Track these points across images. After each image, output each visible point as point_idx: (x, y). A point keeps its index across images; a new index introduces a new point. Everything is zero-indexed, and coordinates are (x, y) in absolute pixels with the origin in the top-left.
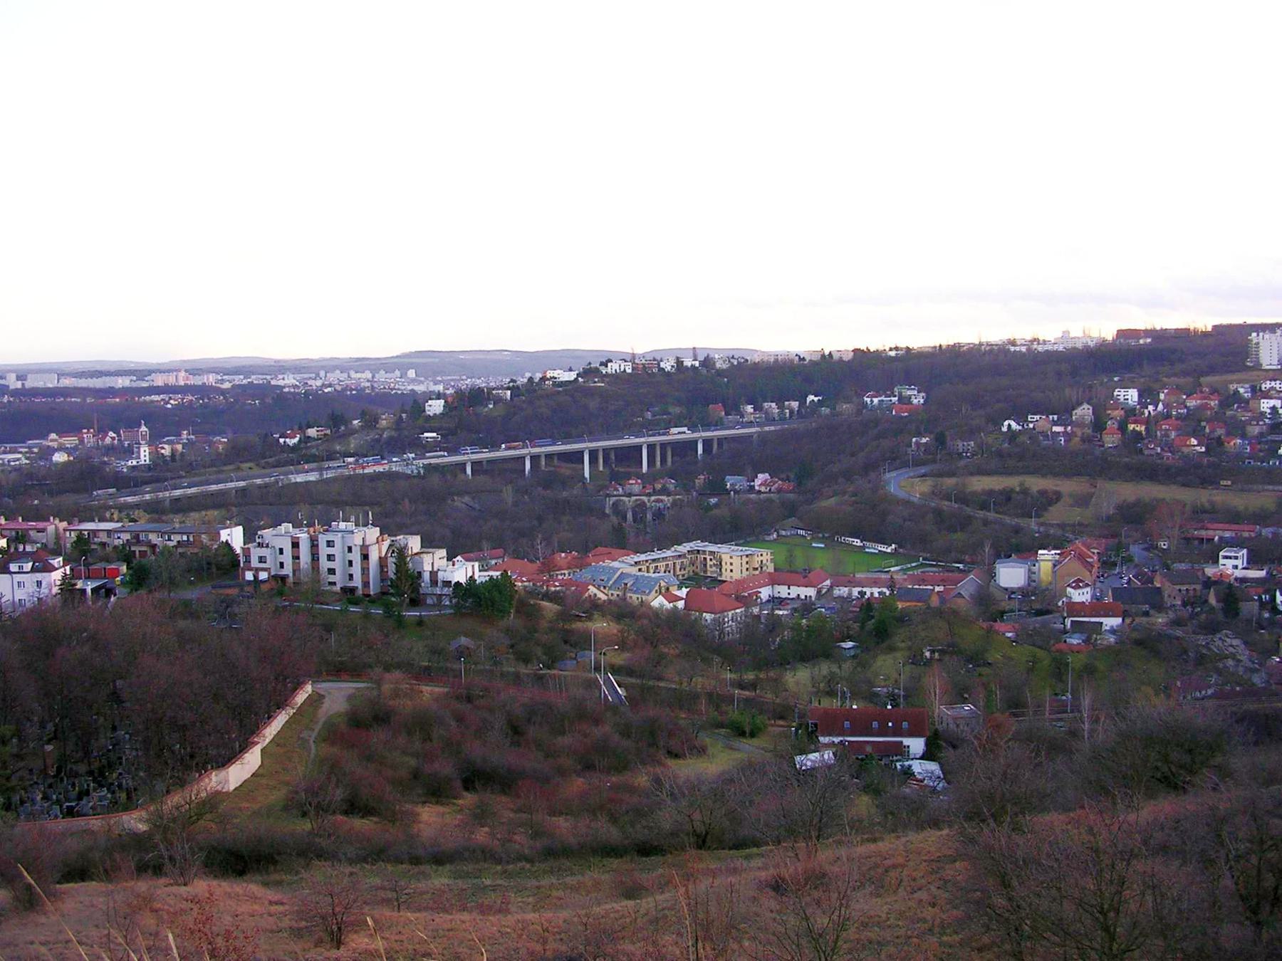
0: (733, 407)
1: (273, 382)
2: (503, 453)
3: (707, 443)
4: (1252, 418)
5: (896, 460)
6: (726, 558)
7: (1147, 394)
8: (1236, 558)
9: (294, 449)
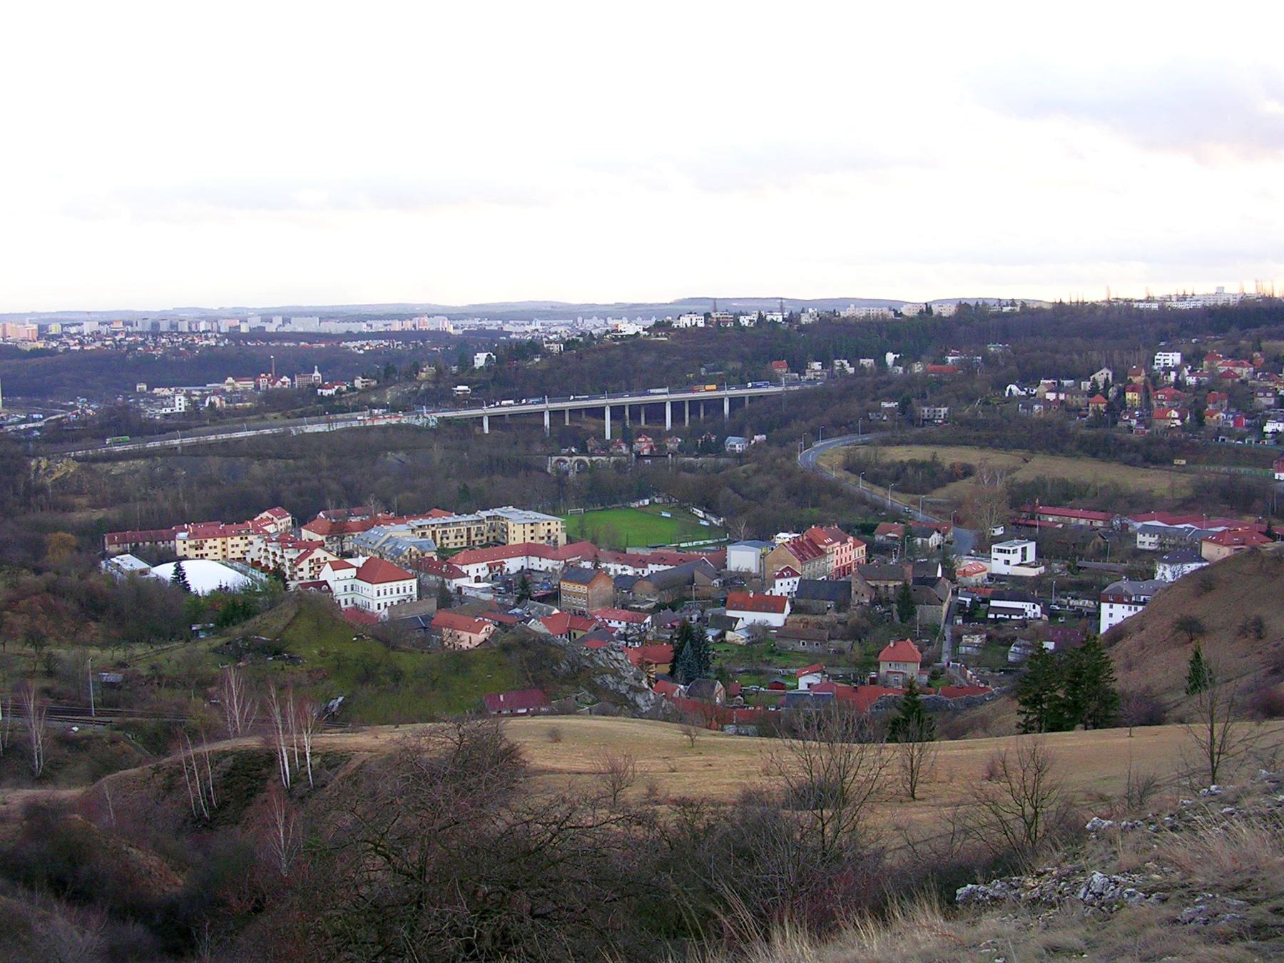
3: (736, 402)
9: (330, 397)
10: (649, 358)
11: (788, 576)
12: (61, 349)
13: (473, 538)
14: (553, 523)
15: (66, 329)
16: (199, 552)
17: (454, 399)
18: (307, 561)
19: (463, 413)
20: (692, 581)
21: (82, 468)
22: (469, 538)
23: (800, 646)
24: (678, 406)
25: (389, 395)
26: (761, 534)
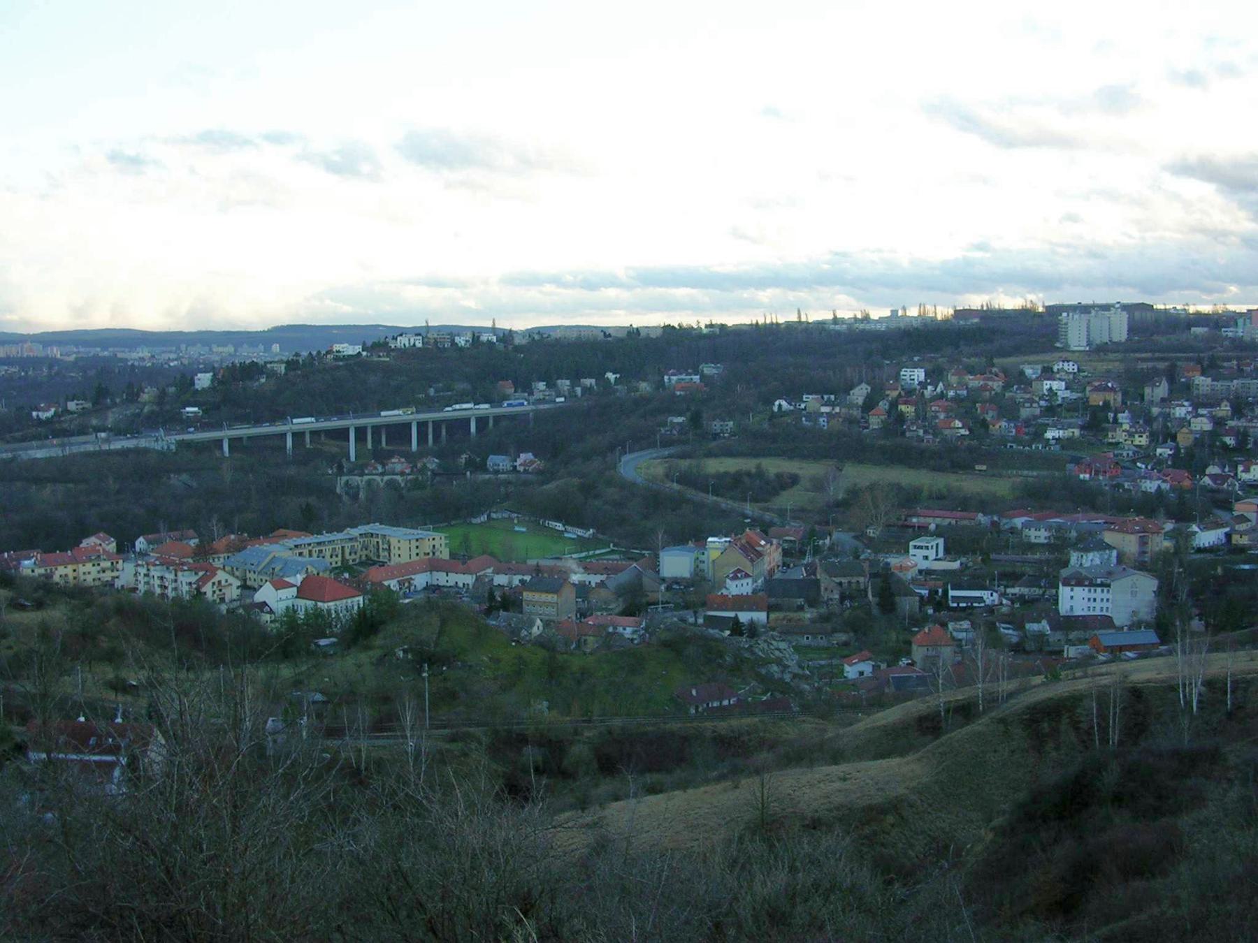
0: (525, 386)
1: (119, 355)
2: (266, 429)
4: (1028, 400)
5: (642, 440)
6: (394, 541)
7: (935, 375)
8: (927, 548)
9: (49, 421)
10: (373, 379)
14: (437, 538)
24: (361, 432)
25: (111, 418)
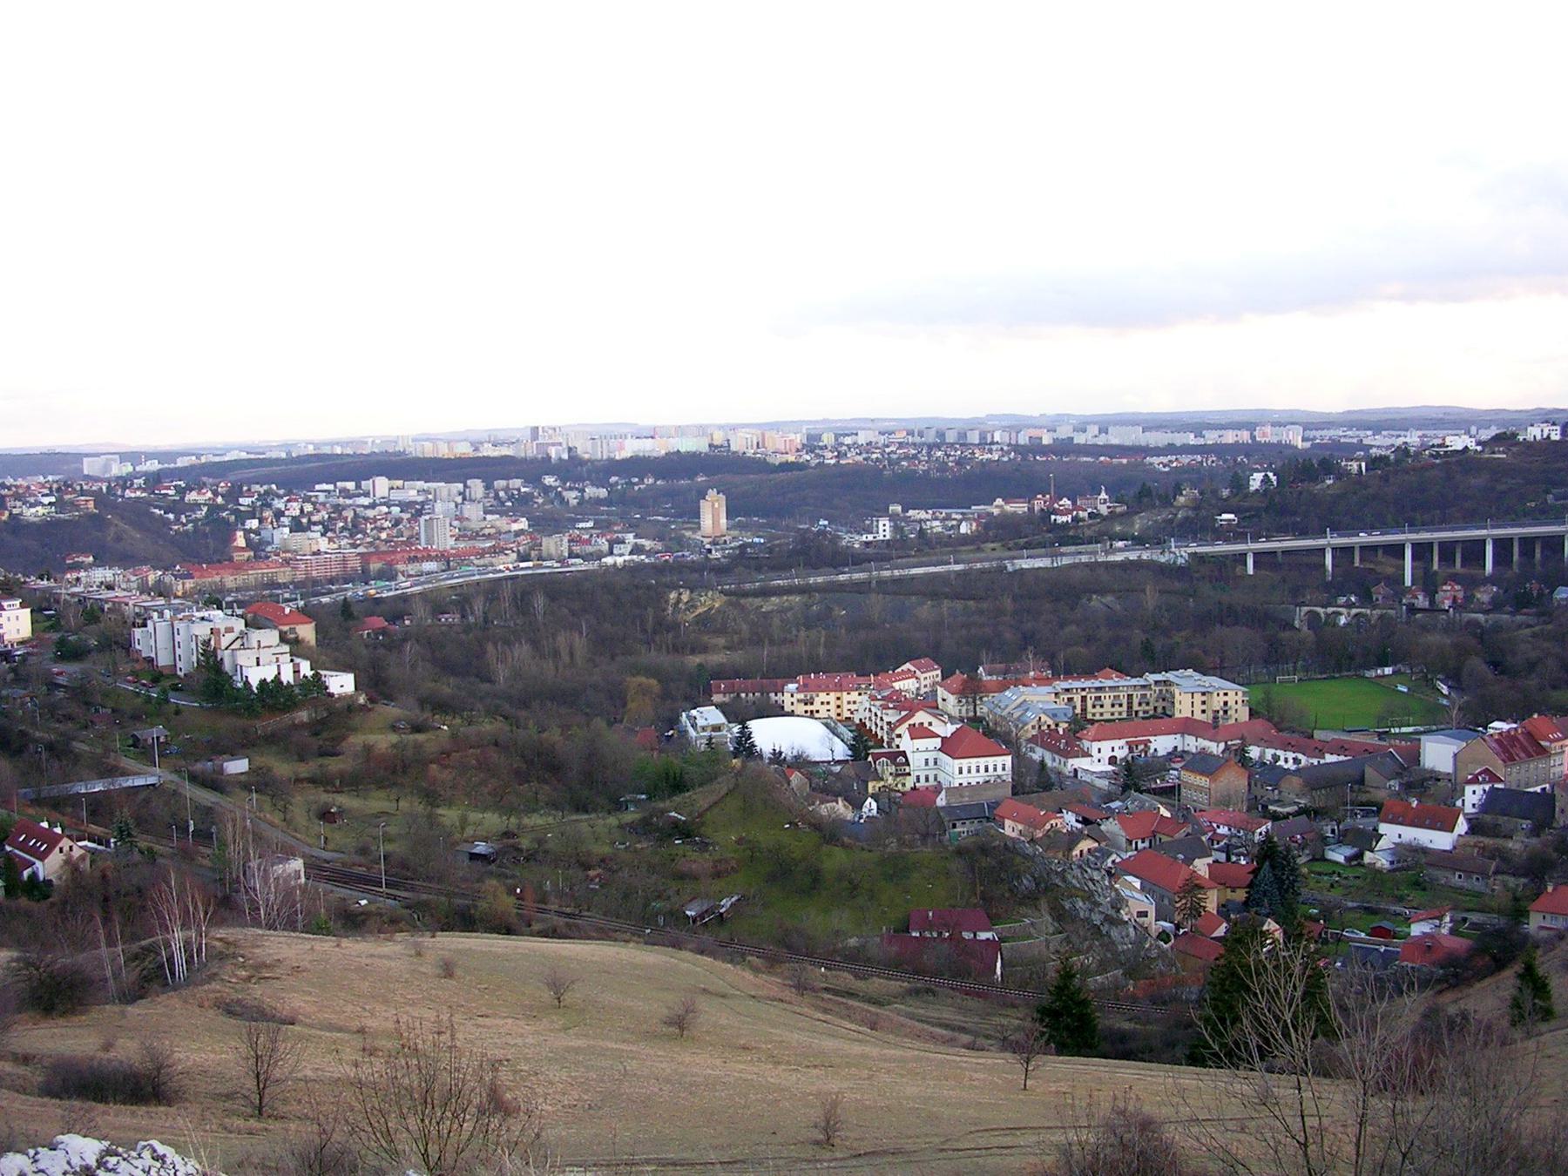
9: (1065, 525)
11: (1484, 782)
12: (814, 462)
13: (1136, 707)
15: (841, 439)
16: (809, 708)
17: (1215, 530)
18: (906, 725)
19: (1222, 548)
20: (1361, 781)
21: (730, 603)
22: (1130, 707)
23: (1455, 880)
24: (1502, 545)
25: (1138, 525)
26: (1472, 721)
